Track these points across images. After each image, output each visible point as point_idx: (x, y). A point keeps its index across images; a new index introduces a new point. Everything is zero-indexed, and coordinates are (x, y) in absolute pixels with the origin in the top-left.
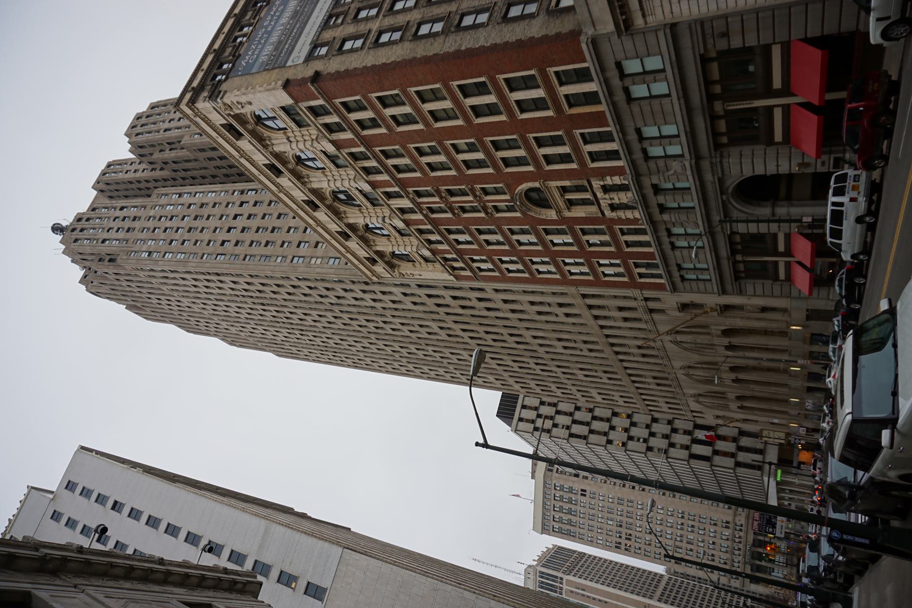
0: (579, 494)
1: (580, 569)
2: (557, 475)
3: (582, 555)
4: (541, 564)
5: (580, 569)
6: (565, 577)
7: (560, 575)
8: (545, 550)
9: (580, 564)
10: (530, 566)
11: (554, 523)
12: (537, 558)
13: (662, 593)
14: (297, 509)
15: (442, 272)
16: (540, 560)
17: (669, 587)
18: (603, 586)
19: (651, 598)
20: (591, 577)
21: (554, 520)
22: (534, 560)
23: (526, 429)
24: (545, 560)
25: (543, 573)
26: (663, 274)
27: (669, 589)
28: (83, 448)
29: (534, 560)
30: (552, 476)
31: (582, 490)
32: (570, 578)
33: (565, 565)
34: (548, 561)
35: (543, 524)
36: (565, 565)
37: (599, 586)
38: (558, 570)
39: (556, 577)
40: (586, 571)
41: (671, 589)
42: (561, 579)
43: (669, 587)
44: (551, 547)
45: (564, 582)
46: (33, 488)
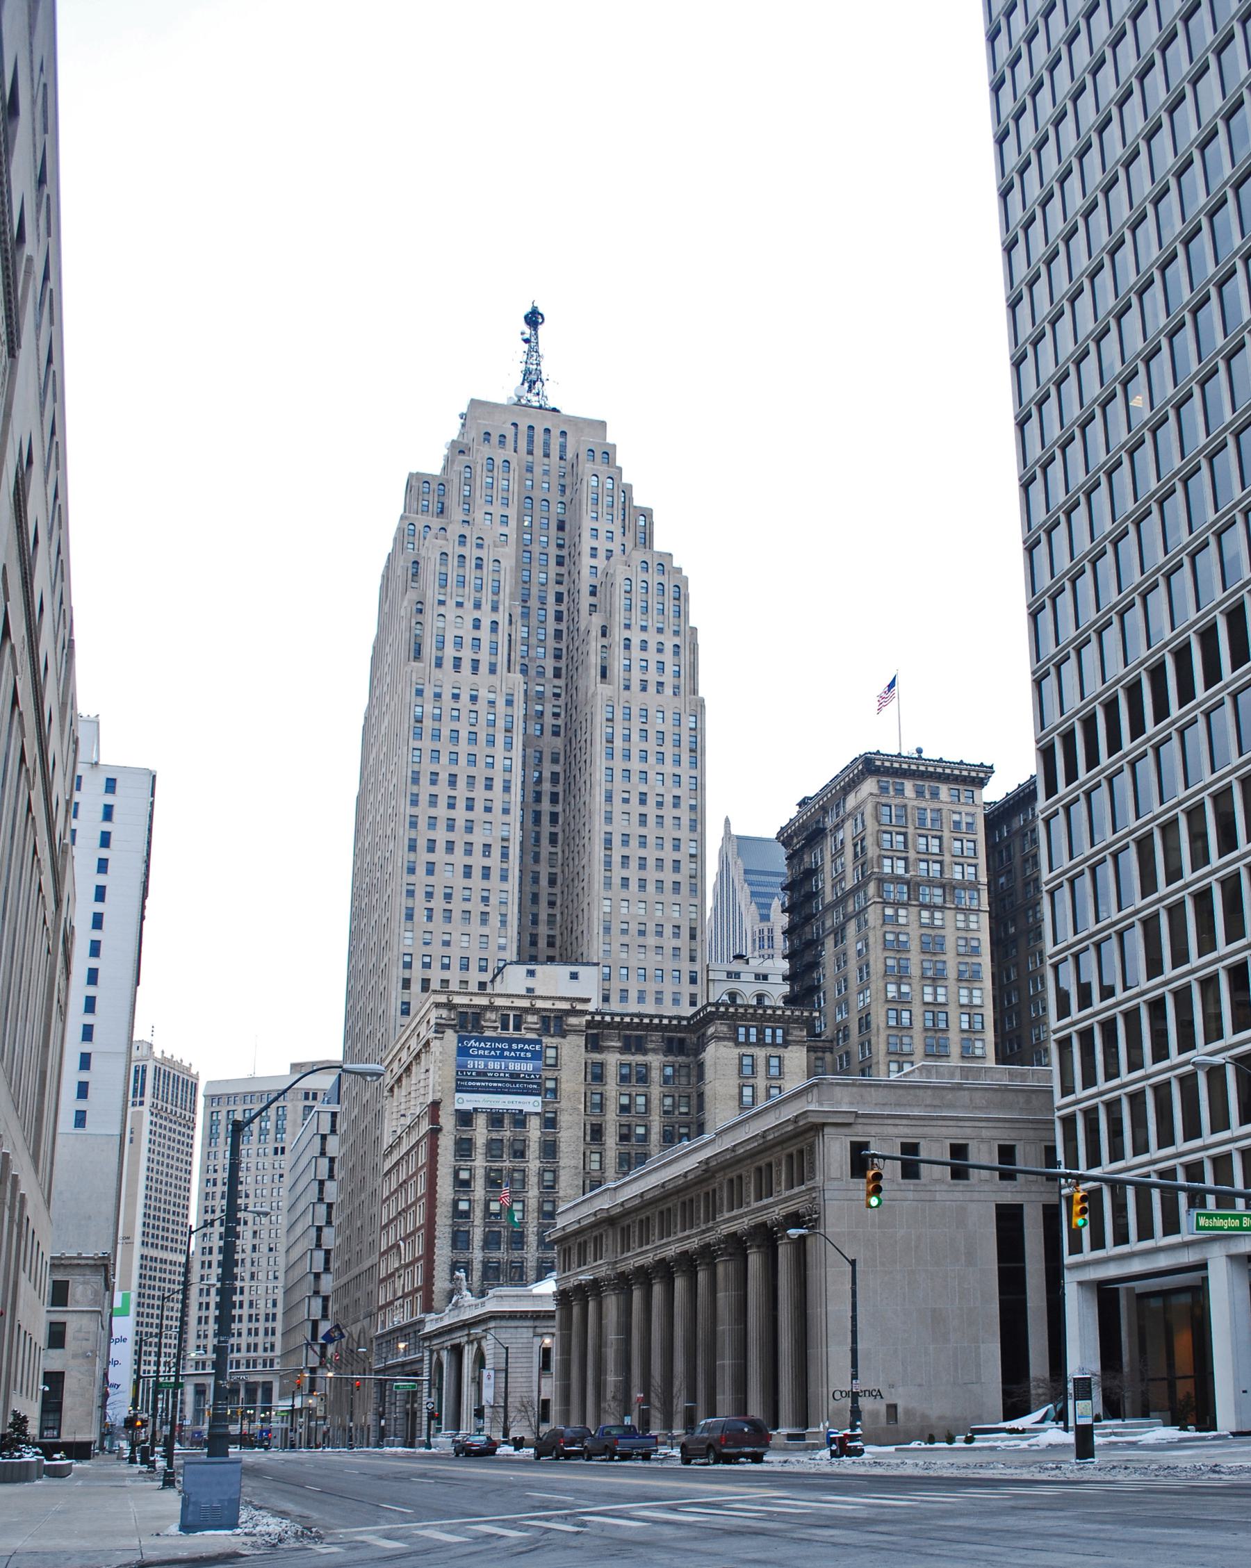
0: (276, 1145)
1: (165, 1129)
2: (300, 1108)
3: (191, 1125)
4: (158, 1065)
5: (165, 1129)
6: (146, 1109)
7: (148, 1099)
8: (186, 1064)
9: (174, 1126)
10: (151, 1046)
11: (224, 1113)
12: (168, 1055)
13: (156, 1258)
14: (147, 902)
15: (287, 1265)
16: (165, 1061)
17: (168, 1267)
18: (145, 1178)
19: (143, 1244)
20: (154, 1185)
21: (229, 1112)
22: (163, 1052)
23: (321, 1123)
24: (167, 1069)
25: (144, 1071)
26: (387, 1329)
27: (164, 1266)
28: (154, 777)
29: (163, 1052)
30: (297, 1100)
31: (283, 1149)
32: (147, 1117)
33: (167, 1102)
34: (167, 1075)
35: (219, 1097)
36: (167, 1102)
37: (144, 1164)
38: (154, 1096)
39: (142, 1095)
40: (164, 1138)
41: (167, 1247)
42: (142, 1103)
43: (168, 1267)
44: (194, 1071)
45: (138, 1108)
46: (98, 723)
